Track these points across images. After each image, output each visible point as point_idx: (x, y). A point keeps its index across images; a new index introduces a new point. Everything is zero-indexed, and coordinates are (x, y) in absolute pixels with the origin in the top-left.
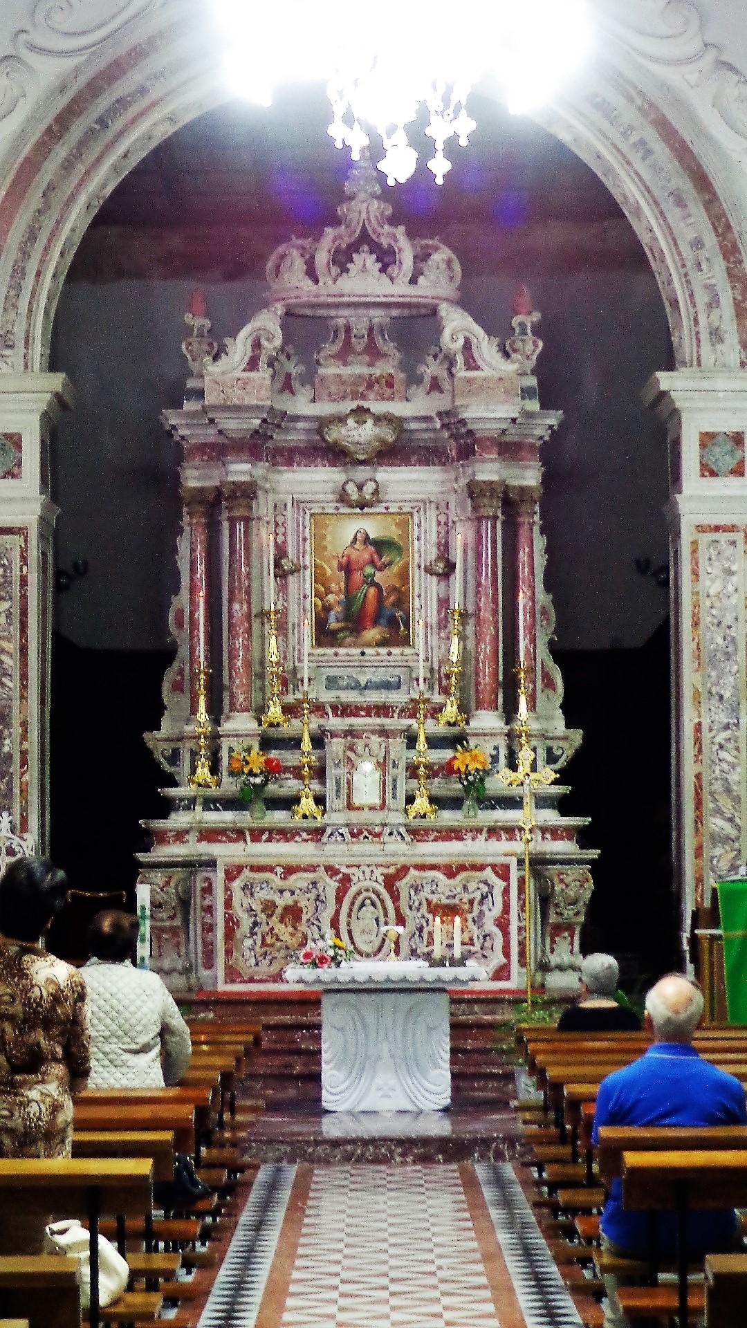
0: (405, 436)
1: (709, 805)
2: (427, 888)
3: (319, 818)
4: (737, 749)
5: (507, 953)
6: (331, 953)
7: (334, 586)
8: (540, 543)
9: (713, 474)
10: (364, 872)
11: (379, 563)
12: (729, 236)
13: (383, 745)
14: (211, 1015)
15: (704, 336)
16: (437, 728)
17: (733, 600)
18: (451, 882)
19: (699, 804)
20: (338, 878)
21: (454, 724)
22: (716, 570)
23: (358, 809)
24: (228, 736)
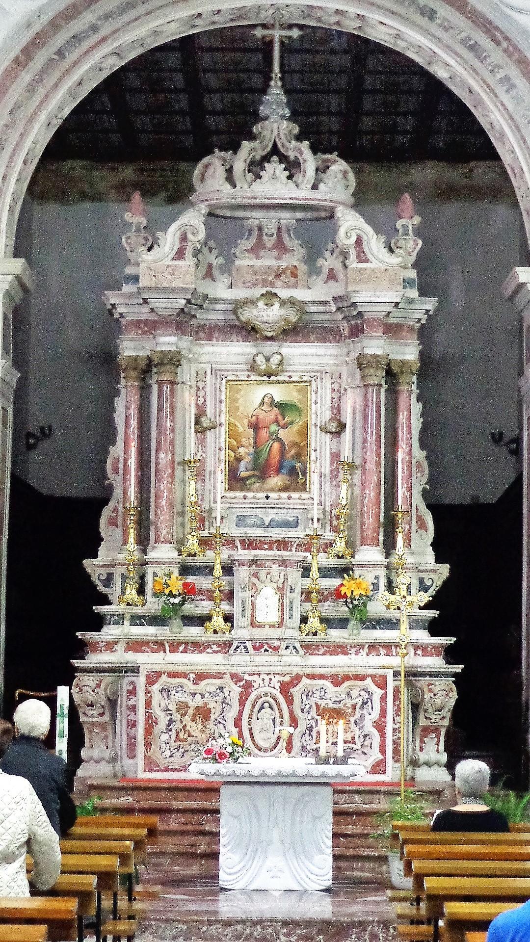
0: (305, 317)
3: (227, 633)
5: (383, 751)
6: (230, 749)
7: (244, 441)
8: (417, 408)
10: (263, 680)
11: (282, 423)
13: (283, 573)
14: (130, 799)
16: (332, 561)
20: (242, 684)
21: (342, 557)
23: (259, 626)
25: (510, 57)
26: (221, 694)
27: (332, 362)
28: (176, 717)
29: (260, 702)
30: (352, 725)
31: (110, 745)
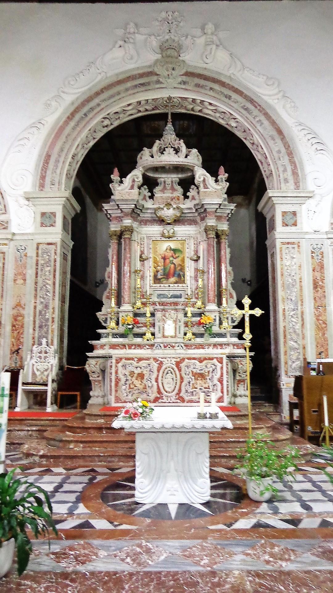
0: (183, 215)
1: (288, 337)
2: (192, 367)
5: (222, 392)
6: (140, 410)
7: (160, 264)
8: (228, 250)
9: (287, 225)
14: (102, 421)
15: (282, 181)
16: (196, 310)
17: (294, 267)
18: (201, 364)
19: (285, 336)
24: (121, 312)
27: (194, 233)
29: (166, 370)
30: (208, 381)
31: (102, 390)
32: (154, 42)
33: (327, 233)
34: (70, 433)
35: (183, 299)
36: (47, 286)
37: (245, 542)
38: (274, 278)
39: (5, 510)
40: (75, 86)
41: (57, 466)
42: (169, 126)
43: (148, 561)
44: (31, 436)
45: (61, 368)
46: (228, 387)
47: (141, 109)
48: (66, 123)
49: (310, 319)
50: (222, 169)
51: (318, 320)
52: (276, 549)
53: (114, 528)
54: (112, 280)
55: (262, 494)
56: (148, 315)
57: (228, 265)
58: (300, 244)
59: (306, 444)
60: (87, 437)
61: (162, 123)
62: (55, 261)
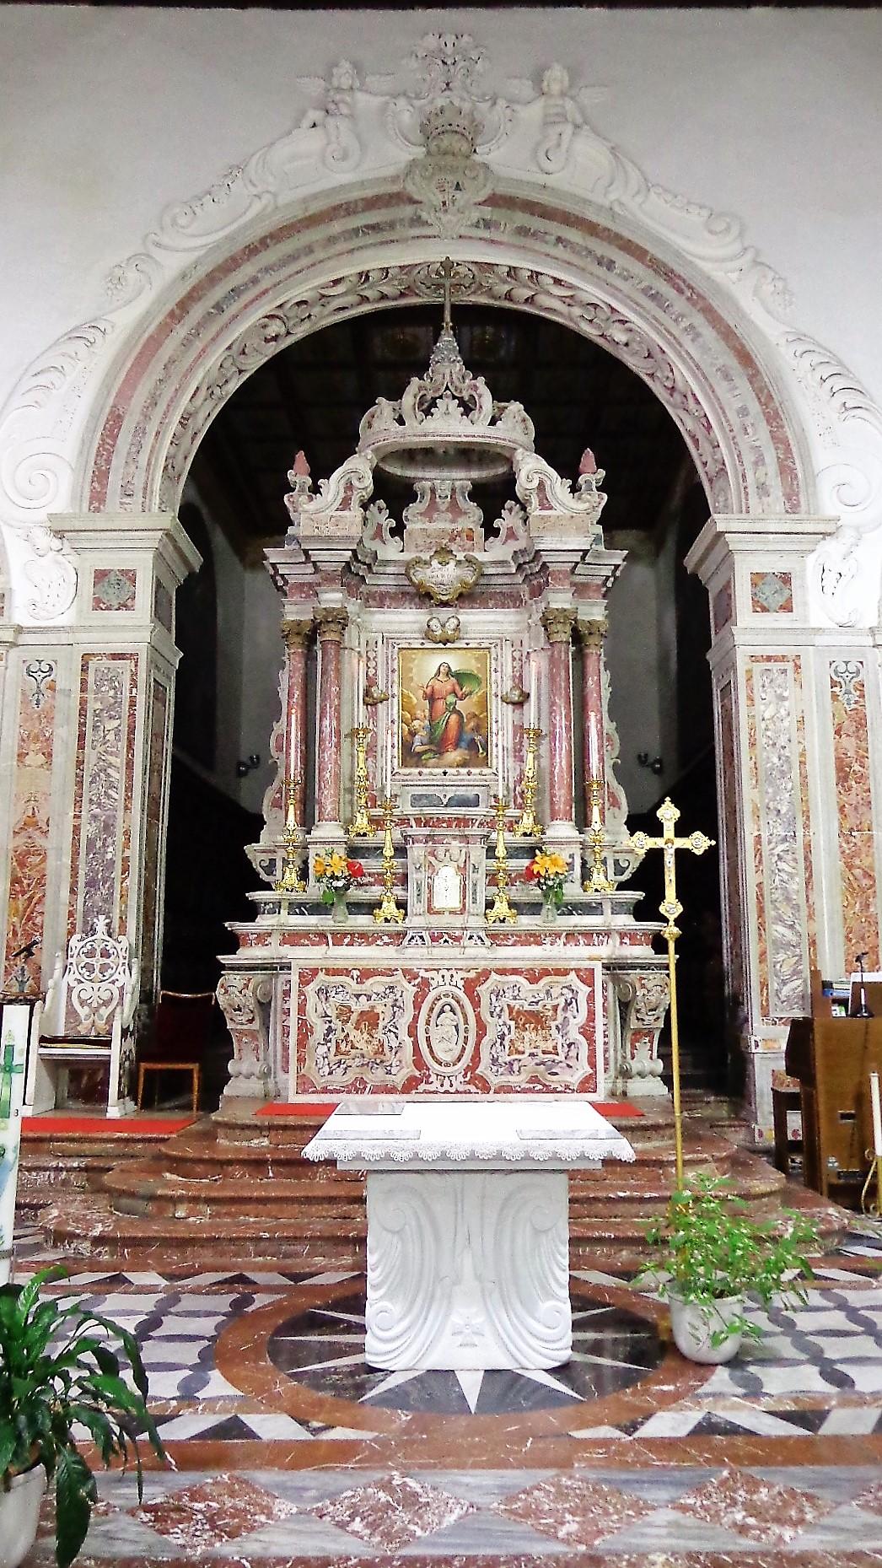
0: (483, 581)
1: (770, 913)
2: (509, 994)
3: (400, 922)
4: (795, 860)
5: (593, 1065)
7: (419, 713)
8: (605, 677)
9: (765, 609)
10: (443, 977)
12: (772, 405)
13: (464, 851)
14: (266, 1142)
15: (752, 490)
16: (518, 840)
17: (786, 724)
18: (534, 987)
19: (761, 911)
20: (416, 982)
22: (770, 696)
23: (438, 913)
24: (316, 843)
25: (694, 305)
26: (391, 995)
27: (515, 628)
28: (337, 1024)
29: (440, 1004)
30: (554, 1031)
31: (261, 1057)
32: (407, 115)
33: (872, 631)
34: (174, 1177)
35: (481, 810)
36: (109, 771)
37: (676, 1474)
38: (730, 754)
39: (23, 1387)
40: (189, 231)
41: (143, 1268)
42: (447, 339)
43: (412, 1527)
44: (65, 1183)
45: (146, 996)
46: (606, 1051)
47: (367, 293)
48: (165, 329)
49: (827, 864)
50: (589, 458)
51: (850, 867)
52: (763, 1494)
53: (312, 1438)
54: (288, 754)
55: (716, 1340)
56: (389, 852)
57: (606, 716)
58: (802, 662)
59: (826, 1206)
60: (223, 1187)
61: (423, 332)
62: (133, 704)
